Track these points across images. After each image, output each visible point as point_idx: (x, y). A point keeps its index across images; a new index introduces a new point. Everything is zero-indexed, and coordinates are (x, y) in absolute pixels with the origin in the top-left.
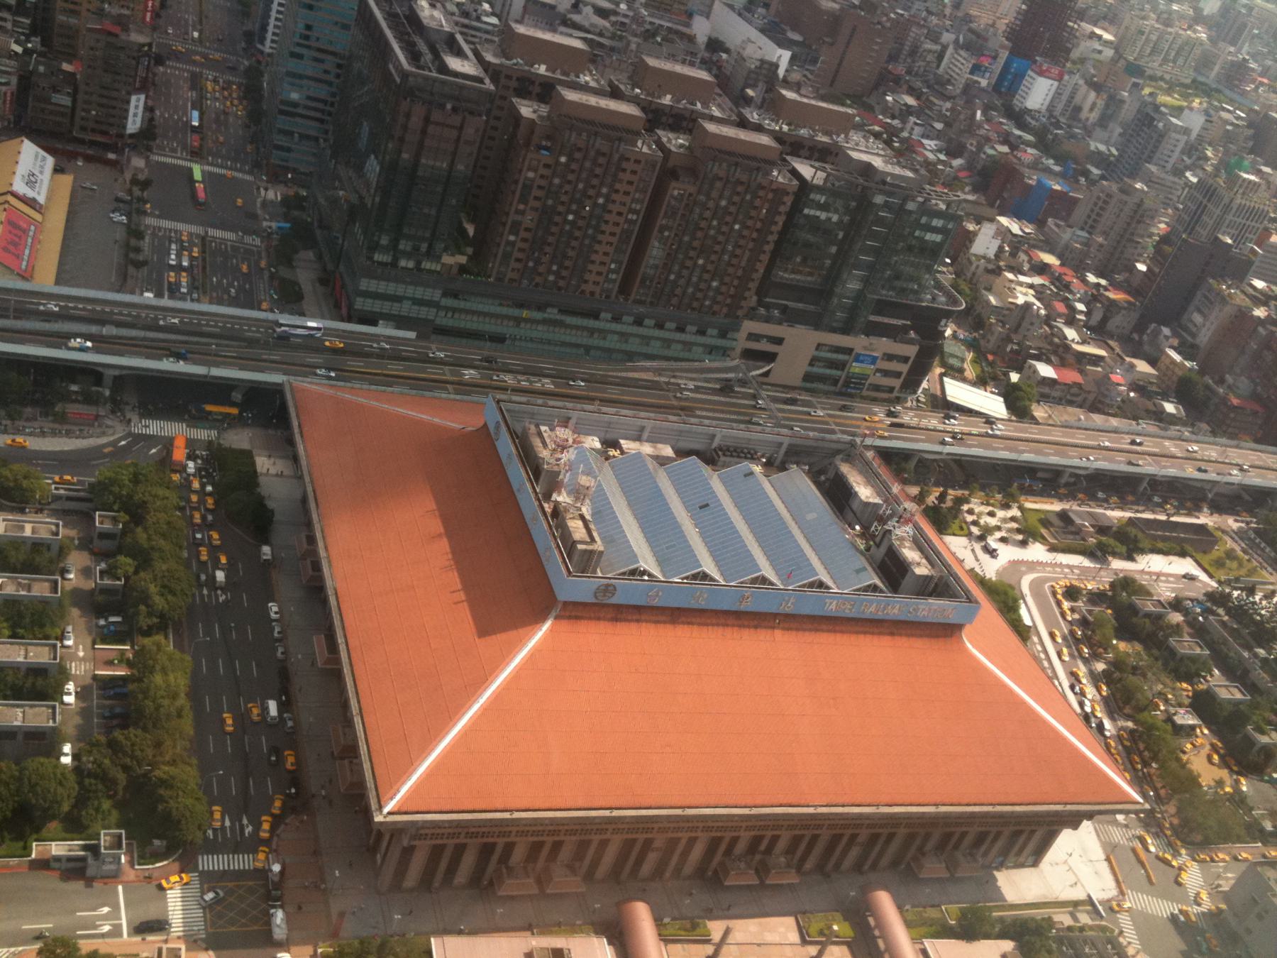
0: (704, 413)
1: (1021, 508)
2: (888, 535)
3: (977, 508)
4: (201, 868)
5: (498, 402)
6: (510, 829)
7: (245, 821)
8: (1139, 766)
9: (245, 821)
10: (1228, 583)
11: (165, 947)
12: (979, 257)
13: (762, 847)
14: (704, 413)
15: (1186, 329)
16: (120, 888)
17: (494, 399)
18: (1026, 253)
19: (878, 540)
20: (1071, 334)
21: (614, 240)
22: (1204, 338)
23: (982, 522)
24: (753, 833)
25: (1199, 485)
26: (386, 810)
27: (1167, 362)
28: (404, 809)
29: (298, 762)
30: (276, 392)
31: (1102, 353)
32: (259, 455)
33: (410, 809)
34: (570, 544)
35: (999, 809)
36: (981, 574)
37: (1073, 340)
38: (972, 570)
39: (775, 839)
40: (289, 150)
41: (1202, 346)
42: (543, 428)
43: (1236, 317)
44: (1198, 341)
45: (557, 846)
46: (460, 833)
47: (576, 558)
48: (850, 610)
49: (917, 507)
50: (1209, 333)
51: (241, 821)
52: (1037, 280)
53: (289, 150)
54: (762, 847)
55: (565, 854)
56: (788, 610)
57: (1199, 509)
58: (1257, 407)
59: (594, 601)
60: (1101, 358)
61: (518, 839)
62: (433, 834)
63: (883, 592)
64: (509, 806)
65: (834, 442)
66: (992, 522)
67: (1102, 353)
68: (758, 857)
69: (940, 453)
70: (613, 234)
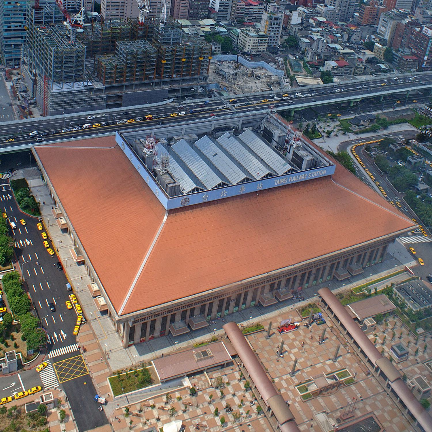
0: (204, 115)
1: (339, 121)
2: (292, 147)
3: (322, 126)
4: (50, 358)
5: (120, 134)
6: (172, 309)
7: (63, 333)
8: (134, 120)
9: (63, 333)
10: (423, 130)
11: (44, 395)
12: (295, 25)
13: (276, 287)
14: (204, 115)
15: (379, 34)
16: (19, 375)
17: (118, 133)
18: (312, 19)
19: (288, 150)
20: (338, 46)
21: (220, 49)
22: (387, 36)
23: (326, 131)
24: (270, 283)
25: (402, 93)
26: (119, 314)
27: (377, 48)
28: (127, 312)
29: (47, 235)
30: (29, 152)
31: (352, 51)
32: (29, 180)
33: (130, 311)
34: (165, 186)
35: (364, 244)
36: (331, 151)
37: (340, 49)
38: (328, 151)
39: (280, 282)
40: (11, 52)
41: (388, 39)
42: (142, 140)
43: (397, 25)
44: (385, 38)
45: (192, 311)
46: (152, 316)
47: (168, 190)
48: (285, 182)
49: (300, 133)
50: (389, 34)
51: (61, 333)
52: (319, 29)
53: (11, 52)
54: (276, 287)
55: (197, 312)
56: (260, 189)
57: (8, 70)
58: (414, 57)
59: (181, 206)
60: (353, 53)
61: (176, 312)
62: (141, 319)
63: (296, 171)
64: (169, 300)
65: (260, 114)
66: (330, 129)
67: (352, 51)
68: (275, 292)
69: (302, 107)
70: (219, 48)
